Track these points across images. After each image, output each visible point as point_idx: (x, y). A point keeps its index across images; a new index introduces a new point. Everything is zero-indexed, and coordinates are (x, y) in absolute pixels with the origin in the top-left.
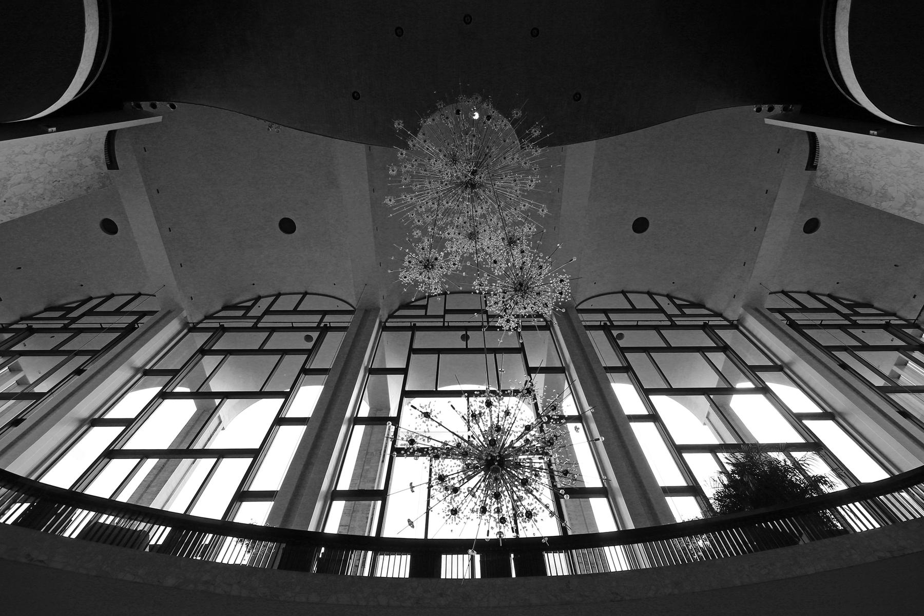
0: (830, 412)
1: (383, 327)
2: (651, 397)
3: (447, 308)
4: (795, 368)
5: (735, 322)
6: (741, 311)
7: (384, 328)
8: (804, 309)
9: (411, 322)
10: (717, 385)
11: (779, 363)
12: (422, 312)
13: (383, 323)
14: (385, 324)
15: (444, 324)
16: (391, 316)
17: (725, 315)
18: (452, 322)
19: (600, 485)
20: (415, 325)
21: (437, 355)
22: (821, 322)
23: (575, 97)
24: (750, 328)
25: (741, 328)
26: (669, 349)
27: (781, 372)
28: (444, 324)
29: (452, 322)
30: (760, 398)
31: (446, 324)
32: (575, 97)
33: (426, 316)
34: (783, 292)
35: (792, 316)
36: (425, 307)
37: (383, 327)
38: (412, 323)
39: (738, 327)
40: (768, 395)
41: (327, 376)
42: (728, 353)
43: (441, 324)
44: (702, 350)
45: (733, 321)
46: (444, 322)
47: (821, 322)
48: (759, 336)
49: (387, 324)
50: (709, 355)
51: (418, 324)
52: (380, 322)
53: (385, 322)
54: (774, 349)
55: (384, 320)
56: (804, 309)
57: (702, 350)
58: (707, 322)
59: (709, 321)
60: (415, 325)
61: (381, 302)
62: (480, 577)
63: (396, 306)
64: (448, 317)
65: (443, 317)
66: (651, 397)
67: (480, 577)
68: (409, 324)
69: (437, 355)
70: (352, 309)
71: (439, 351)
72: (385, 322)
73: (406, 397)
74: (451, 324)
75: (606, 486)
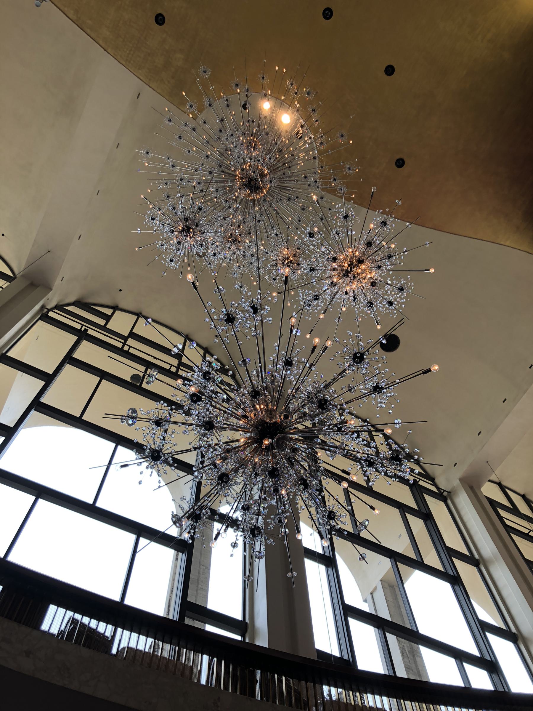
0: (514, 633)
1: (43, 314)
2: (351, 621)
3: (134, 331)
4: (492, 570)
5: (445, 494)
6: (456, 483)
7: (45, 317)
8: (515, 511)
9: (83, 325)
10: (413, 572)
11: (477, 556)
12: (102, 322)
13: (46, 310)
14: (48, 312)
15: (123, 346)
16: (60, 307)
17: (437, 481)
18: (135, 348)
19: (239, 617)
20: (86, 330)
21: (99, 378)
22: (529, 532)
23: (161, 17)
24: (460, 507)
25: (449, 502)
26: (369, 491)
27: (475, 568)
28: (123, 346)
29: (135, 348)
30: (446, 587)
31: (126, 348)
32: (161, 17)
33: (104, 328)
34: (499, 484)
35: (503, 513)
36: (108, 318)
37: (43, 314)
38: (84, 328)
39: (447, 500)
40: (495, 676)
41: (8, 283)
42: (457, 588)
43: (120, 345)
44: (403, 508)
45: (444, 491)
46: (124, 344)
47: (529, 532)
48: (465, 519)
49: (51, 314)
50: (409, 517)
51: (90, 332)
52: (43, 307)
53: (49, 310)
54: (469, 525)
55: (49, 307)
56: (515, 511)
57: (403, 508)
58: (418, 480)
59: (420, 479)
60: (86, 330)
61: (57, 284)
62: (149, 369)
63: (72, 299)
64: (130, 342)
65: (126, 339)
66: (351, 621)
67: (149, 369)
68: (78, 327)
69: (99, 378)
70: (11, 275)
71: (103, 375)
72: (49, 310)
73: (35, 410)
74: (132, 351)
75: (247, 620)
